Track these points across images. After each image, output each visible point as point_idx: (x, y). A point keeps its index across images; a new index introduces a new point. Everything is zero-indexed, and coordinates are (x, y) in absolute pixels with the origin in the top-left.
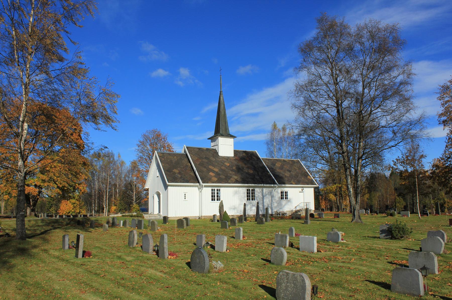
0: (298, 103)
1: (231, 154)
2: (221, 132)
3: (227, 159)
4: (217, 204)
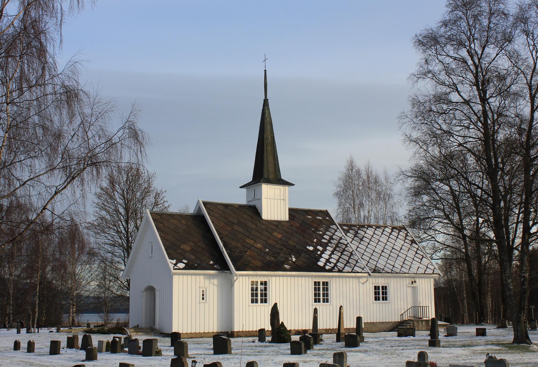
0: (415, 135)
1: (284, 216)
2: (265, 175)
3: (277, 226)
4: (265, 310)
